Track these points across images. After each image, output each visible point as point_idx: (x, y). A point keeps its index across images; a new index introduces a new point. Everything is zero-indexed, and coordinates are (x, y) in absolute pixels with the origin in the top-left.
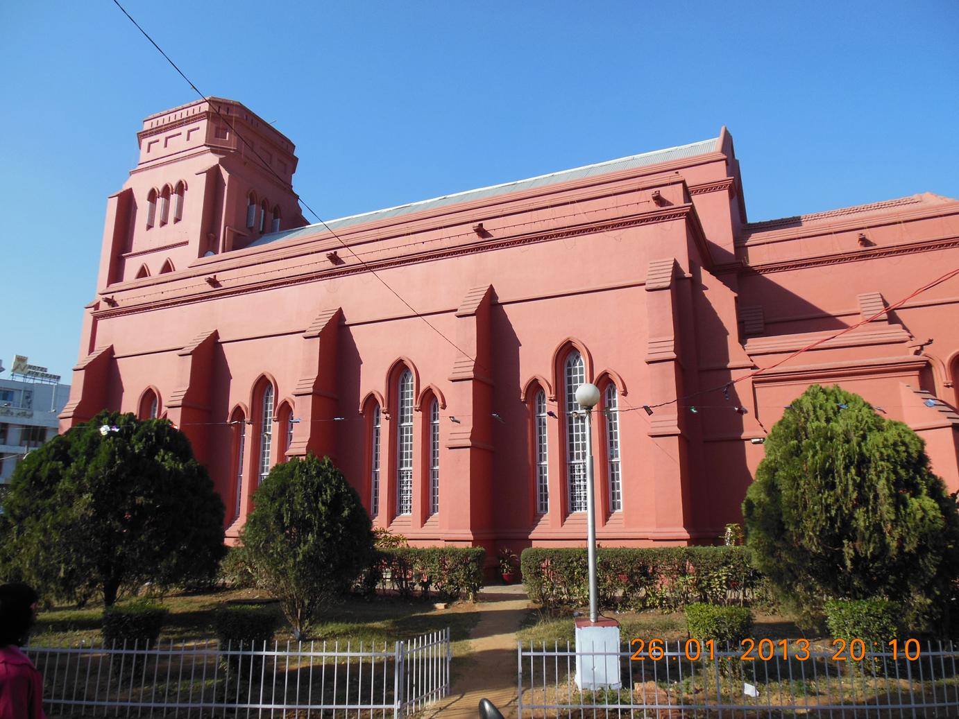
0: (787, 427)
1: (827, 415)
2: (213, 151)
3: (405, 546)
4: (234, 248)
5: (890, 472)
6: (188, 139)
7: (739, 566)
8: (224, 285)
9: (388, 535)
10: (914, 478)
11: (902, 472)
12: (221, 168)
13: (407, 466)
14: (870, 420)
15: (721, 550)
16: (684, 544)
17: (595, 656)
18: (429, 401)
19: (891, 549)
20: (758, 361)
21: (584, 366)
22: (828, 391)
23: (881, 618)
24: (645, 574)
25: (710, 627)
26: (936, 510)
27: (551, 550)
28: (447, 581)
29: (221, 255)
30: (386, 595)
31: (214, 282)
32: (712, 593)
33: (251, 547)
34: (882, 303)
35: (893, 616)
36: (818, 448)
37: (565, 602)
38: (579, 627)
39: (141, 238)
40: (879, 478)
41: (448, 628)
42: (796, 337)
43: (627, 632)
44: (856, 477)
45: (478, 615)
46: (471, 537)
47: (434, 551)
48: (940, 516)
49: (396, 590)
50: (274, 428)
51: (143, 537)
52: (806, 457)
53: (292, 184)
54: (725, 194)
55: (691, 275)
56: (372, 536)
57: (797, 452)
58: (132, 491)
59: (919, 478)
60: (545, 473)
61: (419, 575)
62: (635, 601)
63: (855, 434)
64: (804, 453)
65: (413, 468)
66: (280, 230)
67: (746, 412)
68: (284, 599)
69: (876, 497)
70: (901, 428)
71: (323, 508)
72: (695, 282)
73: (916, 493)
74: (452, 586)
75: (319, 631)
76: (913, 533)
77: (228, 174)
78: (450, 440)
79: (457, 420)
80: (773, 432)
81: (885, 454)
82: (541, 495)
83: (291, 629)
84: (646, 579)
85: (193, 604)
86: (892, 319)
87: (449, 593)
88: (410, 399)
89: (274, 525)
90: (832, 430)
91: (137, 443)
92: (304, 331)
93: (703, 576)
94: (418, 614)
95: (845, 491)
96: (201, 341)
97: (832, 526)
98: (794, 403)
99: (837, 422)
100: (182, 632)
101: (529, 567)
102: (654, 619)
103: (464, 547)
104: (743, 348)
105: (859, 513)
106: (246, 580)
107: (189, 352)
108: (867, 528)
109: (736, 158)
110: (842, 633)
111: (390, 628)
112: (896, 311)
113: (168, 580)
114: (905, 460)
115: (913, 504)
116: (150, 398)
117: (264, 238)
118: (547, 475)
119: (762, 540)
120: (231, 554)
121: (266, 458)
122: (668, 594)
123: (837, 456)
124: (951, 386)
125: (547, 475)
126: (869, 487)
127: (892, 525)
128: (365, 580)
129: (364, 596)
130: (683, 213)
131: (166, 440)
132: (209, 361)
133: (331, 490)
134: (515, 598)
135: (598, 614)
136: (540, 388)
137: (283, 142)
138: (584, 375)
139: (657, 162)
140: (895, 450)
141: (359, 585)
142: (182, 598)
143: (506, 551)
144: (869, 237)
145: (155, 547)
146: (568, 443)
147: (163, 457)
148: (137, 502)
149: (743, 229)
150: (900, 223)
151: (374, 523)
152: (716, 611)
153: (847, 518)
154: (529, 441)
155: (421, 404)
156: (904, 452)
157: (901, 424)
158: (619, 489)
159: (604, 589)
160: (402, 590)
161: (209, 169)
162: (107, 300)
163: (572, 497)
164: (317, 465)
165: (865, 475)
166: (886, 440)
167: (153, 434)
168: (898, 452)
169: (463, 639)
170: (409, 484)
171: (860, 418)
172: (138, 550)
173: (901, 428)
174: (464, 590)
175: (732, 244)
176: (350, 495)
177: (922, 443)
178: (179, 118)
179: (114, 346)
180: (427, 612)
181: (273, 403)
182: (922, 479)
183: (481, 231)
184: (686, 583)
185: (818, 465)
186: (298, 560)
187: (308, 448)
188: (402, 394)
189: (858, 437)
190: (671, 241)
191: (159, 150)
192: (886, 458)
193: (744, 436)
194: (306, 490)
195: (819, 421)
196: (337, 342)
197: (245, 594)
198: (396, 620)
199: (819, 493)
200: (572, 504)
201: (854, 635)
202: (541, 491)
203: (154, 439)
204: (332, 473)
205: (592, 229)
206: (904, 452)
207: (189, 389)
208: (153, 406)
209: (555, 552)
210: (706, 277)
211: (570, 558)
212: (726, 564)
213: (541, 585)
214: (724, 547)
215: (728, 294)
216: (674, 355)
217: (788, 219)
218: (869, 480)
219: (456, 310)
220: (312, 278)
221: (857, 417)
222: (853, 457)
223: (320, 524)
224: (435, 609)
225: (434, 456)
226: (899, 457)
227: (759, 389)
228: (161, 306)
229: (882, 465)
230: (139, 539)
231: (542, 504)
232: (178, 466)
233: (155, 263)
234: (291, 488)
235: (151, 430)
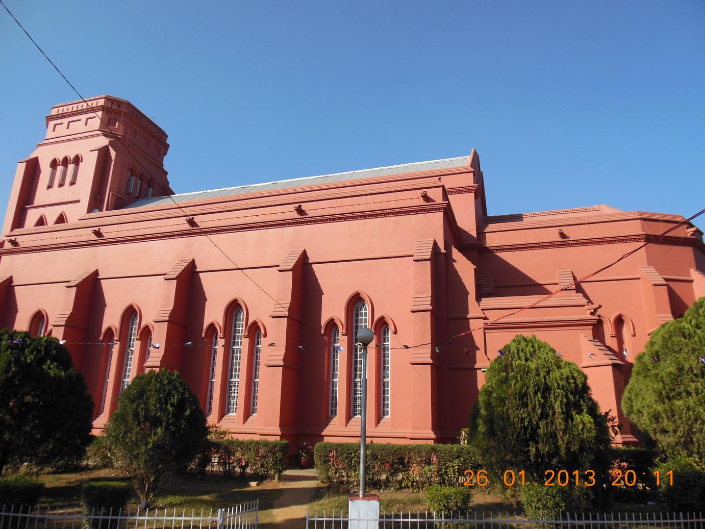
0: (500, 364)
1: (526, 356)
2: (105, 135)
3: (230, 438)
4: (116, 208)
5: (563, 397)
6: (86, 124)
7: (467, 459)
8: (106, 236)
9: (218, 429)
10: (579, 401)
11: (571, 397)
12: (111, 148)
13: (235, 378)
14: (553, 361)
15: (455, 447)
16: (432, 442)
17: (360, 521)
18: (255, 331)
19: (561, 449)
20: (488, 314)
21: (367, 311)
22: (528, 339)
23: (555, 497)
24: (402, 463)
25: (442, 501)
26: (591, 423)
27: (336, 444)
28: (259, 465)
29: (104, 213)
30: (214, 475)
31: (98, 234)
32: (448, 478)
33: (113, 437)
34: (572, 278)
35: (563, 495)
36: (519, 379)
37: (345, 483)
38: (352, 500)
39: (42, 194)
40: (556, 400)
41: (258, 500)
42: (511, 299)
43: (386, 505)
44: (541, 399)
45: (281, 491)
46: (279, 432)
47: (251, 442)
48: (594, 428)
49: (221, 472)
50: (136, 346)
51: (27, 428)
52: (510, 385)
53: (163, 164)
54: (472, 195)
55: (445, 252)
56: (206, 430)
57: (505, 380)
58: (22, 392)
59: (582, 401)
60: (336, 387)
61: (239, 460)
62: (394, 483)
63: (542, 370)
64: (510, 382)
65: (239, 380)
66: (151, 197)
67: (479, 349)
68: (135, 477)
69: (554, 413)
70: (572, 367)
71: (171, 408)
72: (448, 257)
73: (580, 412)
74: (263, 469)
75: (161, 502)
76: (577, 438)
77: (115, 153)
78: (268, 360)
79: (274, 347)
80: (491, 366)
81: (561, 384)
82: (332, 403)
83: (139, 500)
84: (402, 467)
85: (61, 481)
86: (579, 289)
87: (260, 474)
88: (241, 328)
89: (132, 420)
90: (528, 367)
91: (29, 355)
92: (165, 274)
93: (442, 466)
94: (236, 490)
95: (534, 409)
96: (84, 277)
97: (525, 433)
98: (505, 347)
99: (532, 361)
100: (52, 502)
101: (320, 456)
102: (406, 496)
103: (385, 443)
104: (479, 304)
105: (542, 424)
106: (108, 464)
107: (74, 284)
108: (545, 435)
109: (481, 171)
110: (530, 507)
111: (214, 500)
112: (581, 284)
113: (44, 461)
114: (573, 389)
115: (577, 419)
116: (39, 318)
117: (139, 202)
118: (337, 389)
119: (481, 442)
120: (95, 442)
121: (128, 368)
122: (418, 478)
123: (530, 384)
124: (615, 337)
125: (337, 389)
126: (549, 407)
127: (563, 433)
128: (198, 463)
129: (196, 475)
130: (442, 208)
131: (53, 353)
132: (90, 292)
133: (178, 395)
134: (308, 478)
135: (365, 490)
136: (335, 325)
137: (159, 132)
138: (367, 318)
139: (413, 171)
140: (567, 382)
141: (194, 467)
142: (53, 476)
143: (305, 444)
144: (565, 232)
145: (36, 435)
146: (382, 366)
147: (49, 366)
148: (25, 400)
149: (483, 219)
150: (585, 224)
151: (208, 420)
152: (447, 490)
153: (535, 427)
154: (326, 362)
155: (249, 333)
156: (573, 383)
157: (573, 364)
158: (388, 401)
159: (373, 474)
160: (225, 472)
161: (101, 148)
162: (11, 241)
163: (354, 406)
164: (169, 376)
165: (547, 398)
166: (562, 374)
167: (42, 348)
168: (569, 383)
169: (269, 509)
170: (236, 391)
171: (547, 359)
172: (22, 437)
173: (572, 367)
174: (272, 472)
175: (476, 230)
176: (191, 399)
177: (586, 378)
178: (80, 108)
179: (13, 277)
180: (243, 488)
181: (137, 326)
182: (584, 402)
183: (300, 211)
184: (430, 470)
185: (517, 391)
186: (148, 447)
187: (162, 362)
188: (235, 324)
189: (544, 372)
190: (432, 227)
191: (62, 130)
192: (561, 387)
193: (476, 366)
194: (159, 394)
195: (521, 360)
196: (189, 284)
197: (103, 473)
198: (220, 494)
199: (518, 409)
200: (354, 411)
201: (537, 508)
202: (333, 400)
203: (43, 353)
204: (179, 383)
205: (379, 214)
206: (573, 383)
207: (72, 312)
208: (41, 325)
209: (339, 446)
210: (456, 254)
211: (350, 450)
212: (458, 457)
213: (328, 470)
214: (458, 445)
215: (471, 264)
216: (430, 307)
217: (514, 215)
218: (550, 402)
219: (278, 266)
220: (174, 236)
221: (545, 358)
222: (540, 386)
223: (168, 420)
224: (249, 486)
225: (256, 371)
226: (570, 387)
227: (488, 334)
228: (55, 248)
229: (558, 392)
230: (24, 429)
231: (332, 411)
232: (61, 373)
233: (51, 215)
234: (148, 393)
235: (41, 345)
